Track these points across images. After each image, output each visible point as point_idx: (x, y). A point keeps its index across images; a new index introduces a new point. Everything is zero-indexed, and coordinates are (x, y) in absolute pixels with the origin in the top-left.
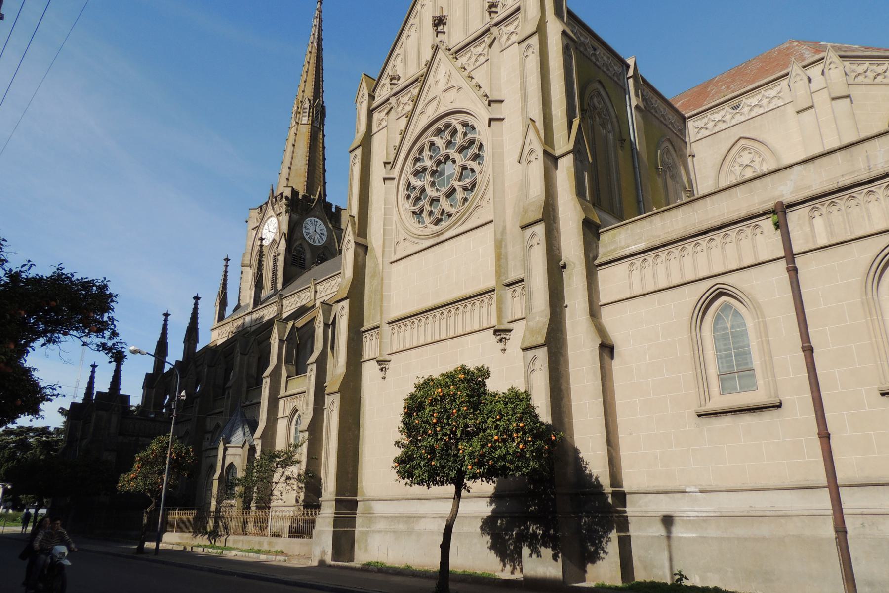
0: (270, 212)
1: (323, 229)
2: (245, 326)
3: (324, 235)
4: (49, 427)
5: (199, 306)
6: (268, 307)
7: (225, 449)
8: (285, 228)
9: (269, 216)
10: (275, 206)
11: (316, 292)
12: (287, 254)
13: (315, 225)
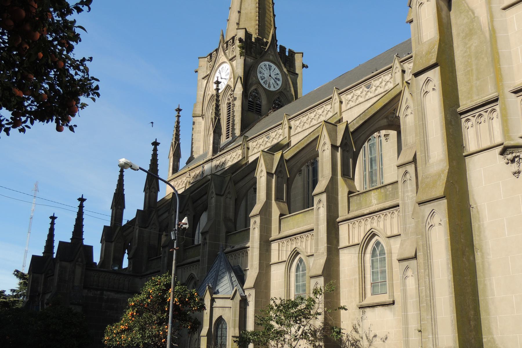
0: (222, 57)
1: (278, 74)
2: (205, 175)
3: (279, 80)
4: (4, 291)
5: (158, 152)
6: (231, 152)
7: (213, 300)
8: (240, 71)
9: (220, 62)
10: (227, 51)
11: (290, 128)
12: (244, 99)
13: (270, 70)
